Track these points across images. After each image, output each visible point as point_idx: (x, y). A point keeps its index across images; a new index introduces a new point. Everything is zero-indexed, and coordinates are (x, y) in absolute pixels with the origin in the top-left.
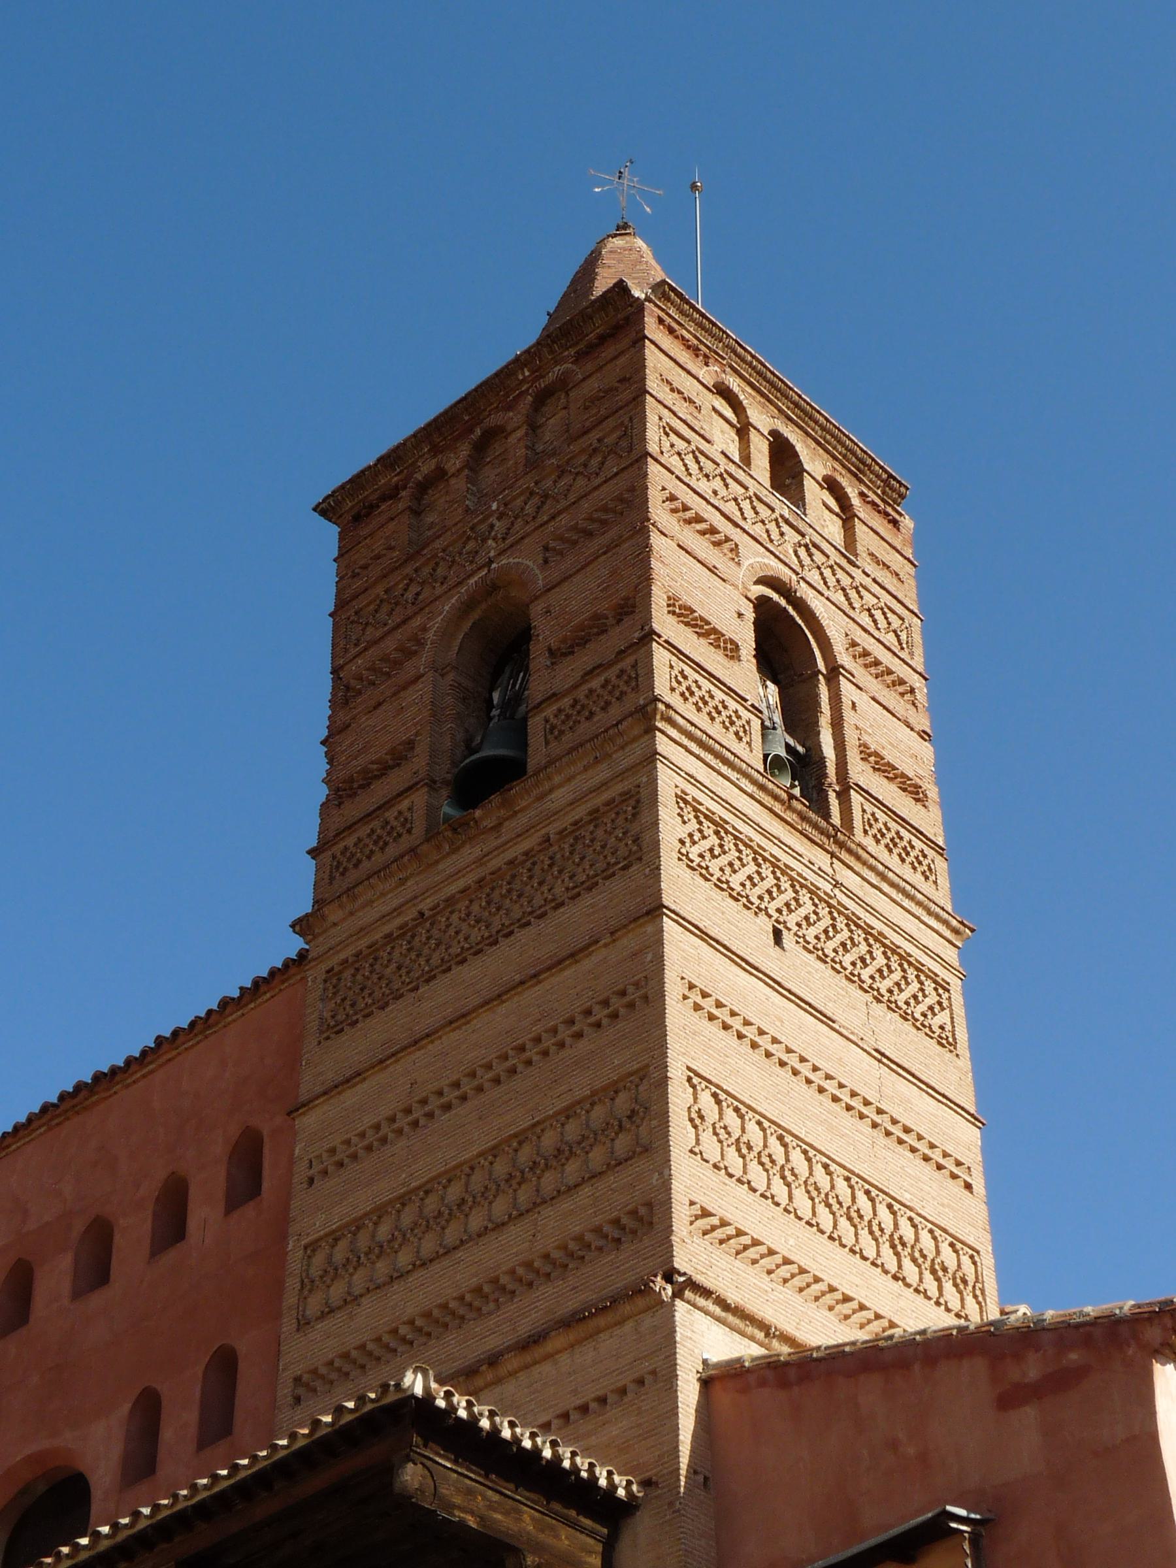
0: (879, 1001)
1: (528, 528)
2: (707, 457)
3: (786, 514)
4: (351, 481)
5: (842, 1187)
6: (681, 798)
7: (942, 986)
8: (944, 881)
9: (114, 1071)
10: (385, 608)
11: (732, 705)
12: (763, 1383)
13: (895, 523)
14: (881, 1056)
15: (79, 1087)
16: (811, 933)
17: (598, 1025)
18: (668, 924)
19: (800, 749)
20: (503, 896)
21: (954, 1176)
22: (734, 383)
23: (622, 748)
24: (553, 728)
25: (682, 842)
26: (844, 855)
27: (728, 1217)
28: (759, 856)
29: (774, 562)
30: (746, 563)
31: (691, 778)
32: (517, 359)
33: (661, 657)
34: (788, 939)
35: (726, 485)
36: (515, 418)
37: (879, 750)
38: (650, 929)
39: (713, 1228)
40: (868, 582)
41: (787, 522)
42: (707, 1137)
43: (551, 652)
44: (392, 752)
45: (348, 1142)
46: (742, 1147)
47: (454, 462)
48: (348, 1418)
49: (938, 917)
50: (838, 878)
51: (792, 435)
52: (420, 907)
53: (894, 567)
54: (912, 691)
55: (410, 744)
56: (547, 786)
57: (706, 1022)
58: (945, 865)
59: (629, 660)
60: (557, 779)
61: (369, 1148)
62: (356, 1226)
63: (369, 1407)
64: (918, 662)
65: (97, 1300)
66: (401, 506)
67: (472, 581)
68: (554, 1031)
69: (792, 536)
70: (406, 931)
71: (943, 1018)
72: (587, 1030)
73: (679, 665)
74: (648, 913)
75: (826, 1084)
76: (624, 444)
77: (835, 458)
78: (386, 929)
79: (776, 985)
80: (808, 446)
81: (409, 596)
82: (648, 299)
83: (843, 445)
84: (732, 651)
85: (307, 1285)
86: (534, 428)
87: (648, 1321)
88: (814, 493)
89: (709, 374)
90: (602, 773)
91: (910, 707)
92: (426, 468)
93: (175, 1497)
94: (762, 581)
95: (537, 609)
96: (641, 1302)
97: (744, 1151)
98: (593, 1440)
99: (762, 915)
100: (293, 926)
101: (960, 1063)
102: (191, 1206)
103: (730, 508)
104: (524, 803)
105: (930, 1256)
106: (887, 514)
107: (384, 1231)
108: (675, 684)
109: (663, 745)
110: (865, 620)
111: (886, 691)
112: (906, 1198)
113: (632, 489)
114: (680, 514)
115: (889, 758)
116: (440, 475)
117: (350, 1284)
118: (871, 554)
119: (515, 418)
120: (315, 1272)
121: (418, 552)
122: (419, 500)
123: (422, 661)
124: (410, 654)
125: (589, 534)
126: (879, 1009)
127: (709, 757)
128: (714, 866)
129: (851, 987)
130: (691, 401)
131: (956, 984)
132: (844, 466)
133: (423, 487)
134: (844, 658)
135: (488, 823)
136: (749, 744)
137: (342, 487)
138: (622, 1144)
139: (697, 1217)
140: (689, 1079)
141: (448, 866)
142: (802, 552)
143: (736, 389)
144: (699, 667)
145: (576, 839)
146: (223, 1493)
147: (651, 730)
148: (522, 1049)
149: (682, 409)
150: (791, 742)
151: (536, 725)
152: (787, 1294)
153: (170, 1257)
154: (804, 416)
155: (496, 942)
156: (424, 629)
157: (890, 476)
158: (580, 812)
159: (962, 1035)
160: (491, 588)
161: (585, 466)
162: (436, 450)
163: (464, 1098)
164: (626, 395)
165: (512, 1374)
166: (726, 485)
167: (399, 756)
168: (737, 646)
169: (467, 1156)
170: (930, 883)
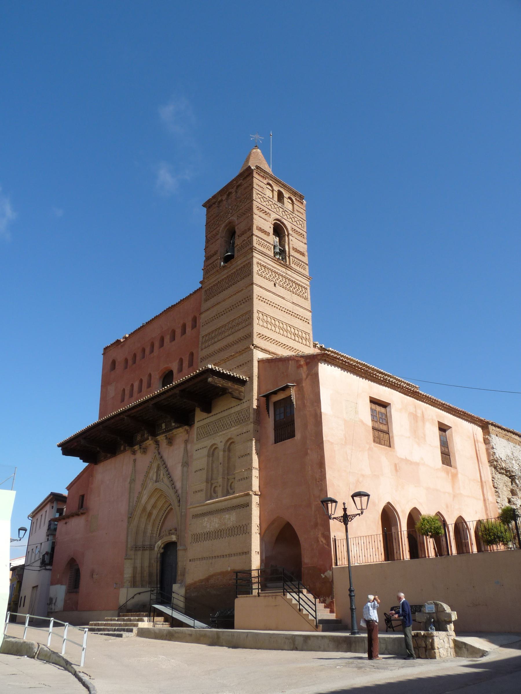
0: (293, 293)
1: (235, 212)
2: (265, 198)
3: (280, 206)
4: (208, 201)
5: (285, 326)
6: (258, 263)
7: (306, 289)
8: (307, 270)
9: (174, 305)
10: (214, 225)
11: (268, 244)
12: (266, 362)
13: (302, 203)
14: (293, 303)
15: (169, 308)
16: (281, 283)
17: (244, 302)
18: (254, 286)
19: (282, 249)
20: (231, 279)
21: (306, 322)
22: (271, 182)
23: (248, 254)
24: (238, 250)
25: (258, 271)
26: (288, 269)
27: (264, 334)
28: (272, 271)
29: (277, 216)
30: (272, 217)
31: (259, 259)
32: (233, 180)
33: (255, 238)
34: (277, 285)
35: (269, 203)
36: (233, 190)
37: (296, 248)
38: (252, 287)
39: (261, 336)
40: (296, 216)
41: (280, 207)
42: (260, 321)
43: (238, 236)
44: (215, 252)
45: (208, 320)
46: (267, 322)
47: (224, 198)
48: (201, 371)
49: (305, 277)
50: (287, 273)
51: (282, 190)
52: (219, 280)
53: (301, 212)
54: (304, 235)
55: (217, 251)
56: (237, 260)
57: (261, 302)
58: (308, 267)
59: (250, 238)
60: (239, 259)
61: (211, 321)
62: (209, 334)
63: (203, 370)
64: (305, 230)
65: (173, 343)
66: (216, 206)
67: (227, 221)
68: (238, 303)
69: (282, 210)
70: (217, 284)
71: (306, 294)
72: (242, 303)
73: (258, 239)
74: (251, 284)
75: (283, 309)
76: (250, 197)
77: (291, 193)
78: (214, 284)
79: (274, 293)
80: (285, 192)
81: (217, 223)
82: (254, 169)
83: (292, 190)
84: (268, 234)
85: (202, 343)
86: (236, 192)
87: (250, 352)
88: (286, 200)
89: (265, 182)
90: (245, 259)
91: (303, 238)
92: (220, 199)
93: (178, 381)
94: (275, 220)
95: (236, 228)
96: (249, 349)
97: (267, 323)
98: (242, 371)
99: (272, 282)
100: (200, 282)
101: (308, 302)
102: (186, 328)
103: (269, 207)
104: (234, 263)
105: (301, 336)
106: (301, 202)
107: (213, 335)
108: (257, 242)
109: (254, 254)
110: (295, 223)
111: (298, 236)
112: (297, 327)
113: (251, 206)
114: (259, 210)
115: (298, 249)
116: (222, 200)
117: (208, 343)
118: (297, 210)
119: (233, 190)
120: (203, 341)
121: (218, 215)
122: (219, 204)
123: (219, 236)
124: (217, 234)
125: (245, 214)
126: (293, 295)
127: (263, 255)
128: (263, 274)
129: (288, 291)
130: (262, 187)
131: (308, 288)
132: (292, 194)
133: (220, 202)
134: (290, 232)
135: (228, 266)
136: (271, 251)
137: (206, 202)
138: (247, 323)
139: (258, 335)
140: (257, 312)
141: (223, 273)
142: (283, 213)
143: (271, 183)
144: (262, 239)
145: (241, 270)
146: (184, 381)
147: (253, 252)
148: (233, 306)
149: (260, 189)
150: (280, 248)
151: (236, 249)
152: (274, 345)
153: (184, 336)
154: (284, 186)
155: (229, 287)
156: (220, 230)
157: (301, 195)
158: (242, 265)
159: (309, 297)
160: (230, 223)
161: (244, 201)
162: (221, 196)
163: (224, 313)
164: (250, 188)
165: (231, 359)
166: (269, 203)
167: (216, 253)
168: (269, 233)
169: (225, 323)
170: (305, 271)
